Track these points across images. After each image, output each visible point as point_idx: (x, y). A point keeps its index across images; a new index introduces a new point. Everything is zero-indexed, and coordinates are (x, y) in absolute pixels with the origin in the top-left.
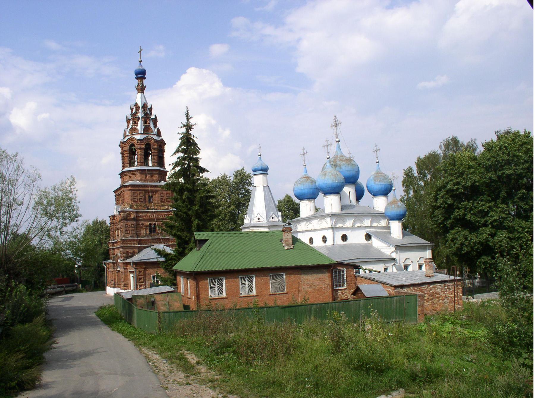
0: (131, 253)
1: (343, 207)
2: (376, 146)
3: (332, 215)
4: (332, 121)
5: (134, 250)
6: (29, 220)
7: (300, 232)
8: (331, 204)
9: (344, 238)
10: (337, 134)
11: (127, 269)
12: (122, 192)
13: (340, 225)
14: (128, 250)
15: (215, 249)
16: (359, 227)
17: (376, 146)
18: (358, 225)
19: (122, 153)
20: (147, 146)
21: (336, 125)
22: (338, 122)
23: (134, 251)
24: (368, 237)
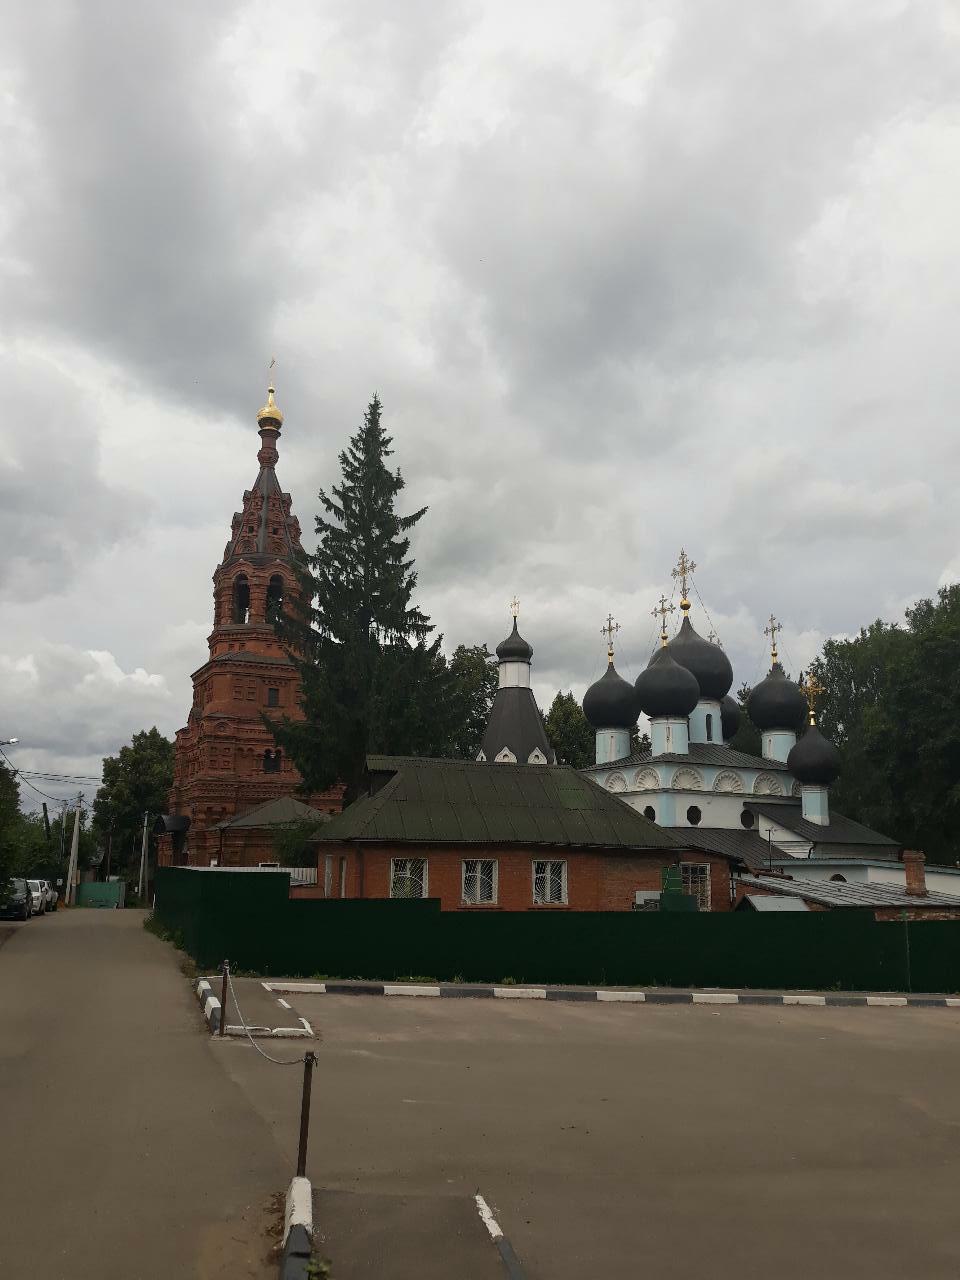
0: (216, 813)
1: (693, 747)
2: (773, 619)
3: (668, 760)
4: (675, 564)
5: (211, 804)
6: (885, 895)
7: (46, 815)
8: (663, 735)
9: (694, 814)
10: (684, 590)
11: (205, 848)
12: (210, 677)
13: (728, 788)
14: (211, 804)
15: (411, 792)
16: (726, 794)
17: (773, 619)
18: (727, 787)
19: (217, 595)
20: (274, 583)
21: (684, 570)
22: (613, 625)
23: (224, 809)
24: (748, 817)
